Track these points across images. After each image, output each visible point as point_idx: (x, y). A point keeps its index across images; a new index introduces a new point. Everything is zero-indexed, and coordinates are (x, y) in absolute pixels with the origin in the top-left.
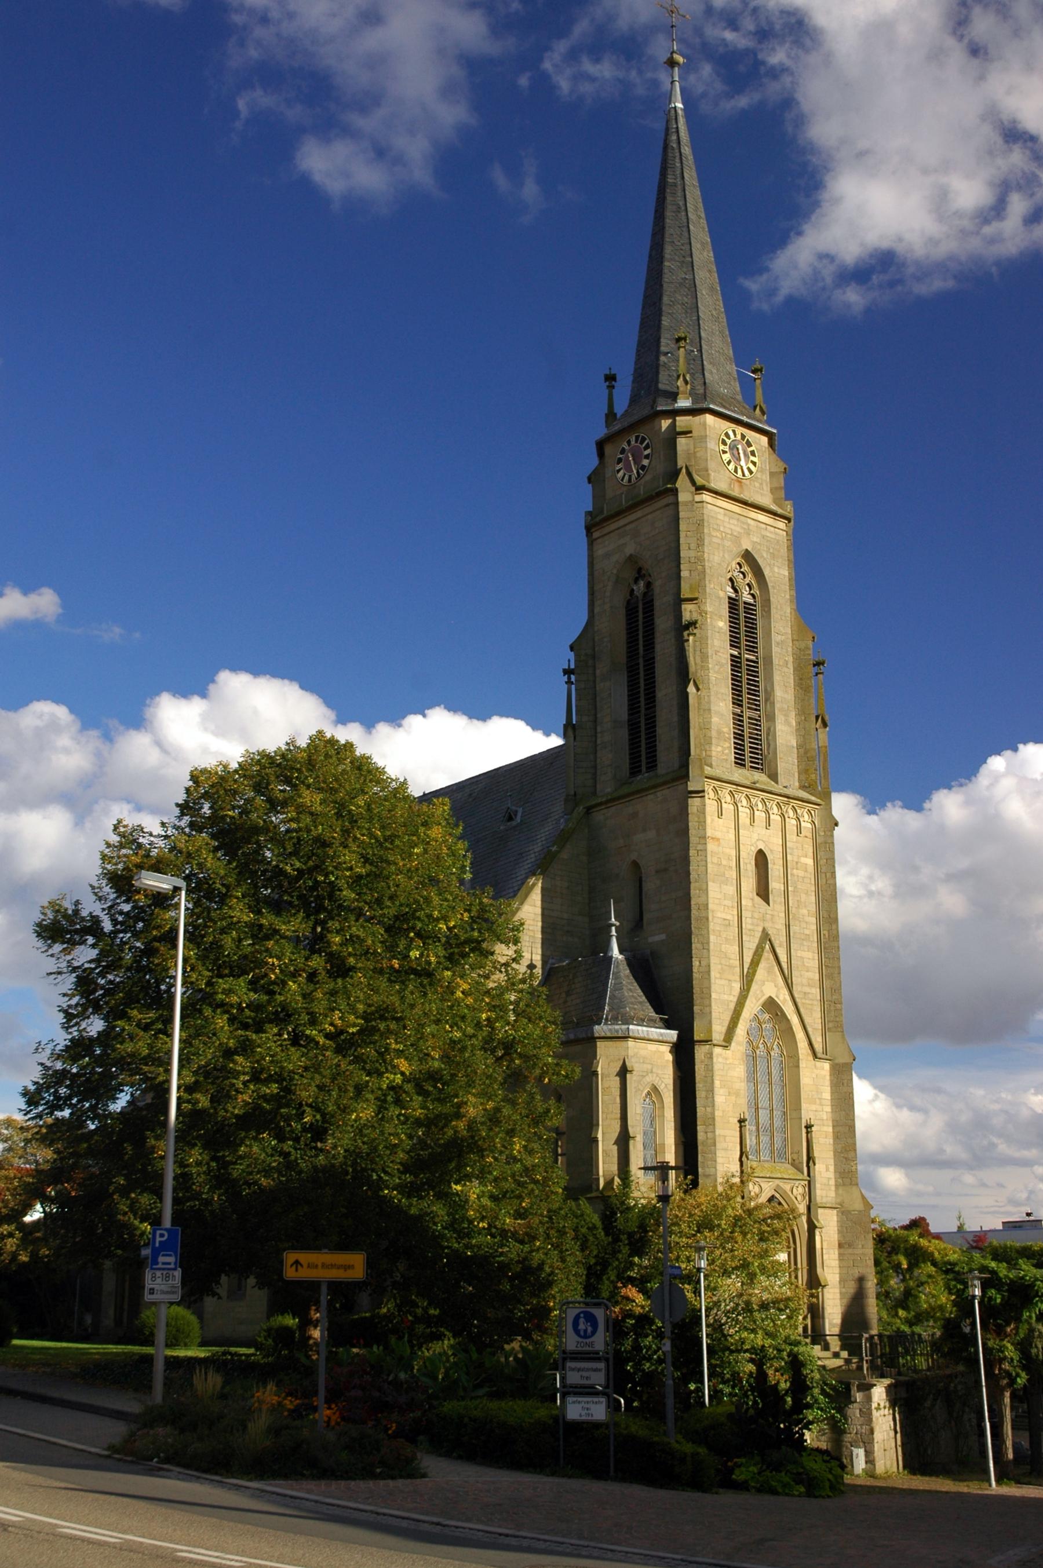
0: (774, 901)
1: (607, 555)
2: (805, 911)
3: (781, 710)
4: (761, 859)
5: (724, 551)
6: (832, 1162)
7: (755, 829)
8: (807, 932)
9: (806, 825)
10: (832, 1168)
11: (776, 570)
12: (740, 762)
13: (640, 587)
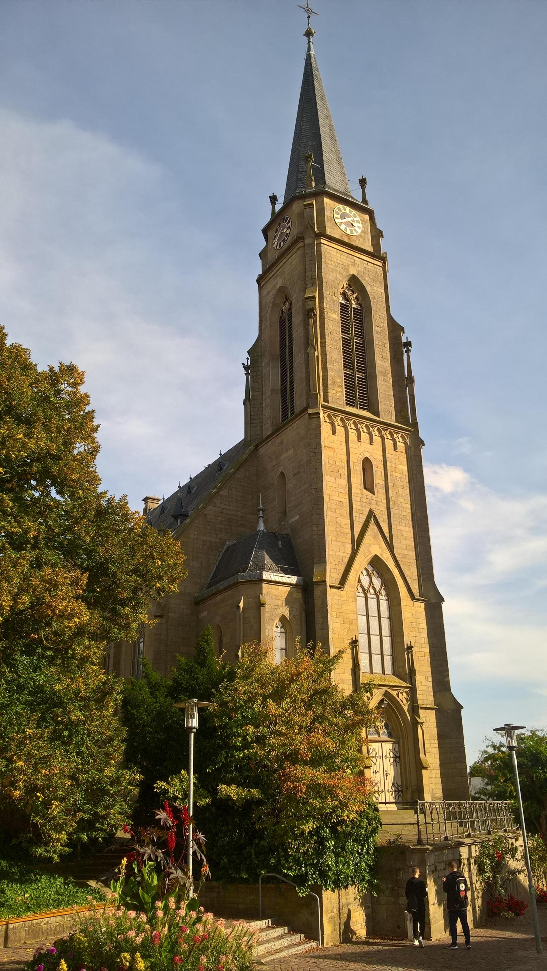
0: (378, 492)
1: (268, 294)
2: (402, 500)
3: (381, 372)
4: (367, 463)
5: (336, 273)
6: (430, 674)
7: (362, 444)
8: (405, 514)
9: (401, 446)
10: (430, 679)
11: (375, 288)
12: (350, 402)
13: (285, 308)
